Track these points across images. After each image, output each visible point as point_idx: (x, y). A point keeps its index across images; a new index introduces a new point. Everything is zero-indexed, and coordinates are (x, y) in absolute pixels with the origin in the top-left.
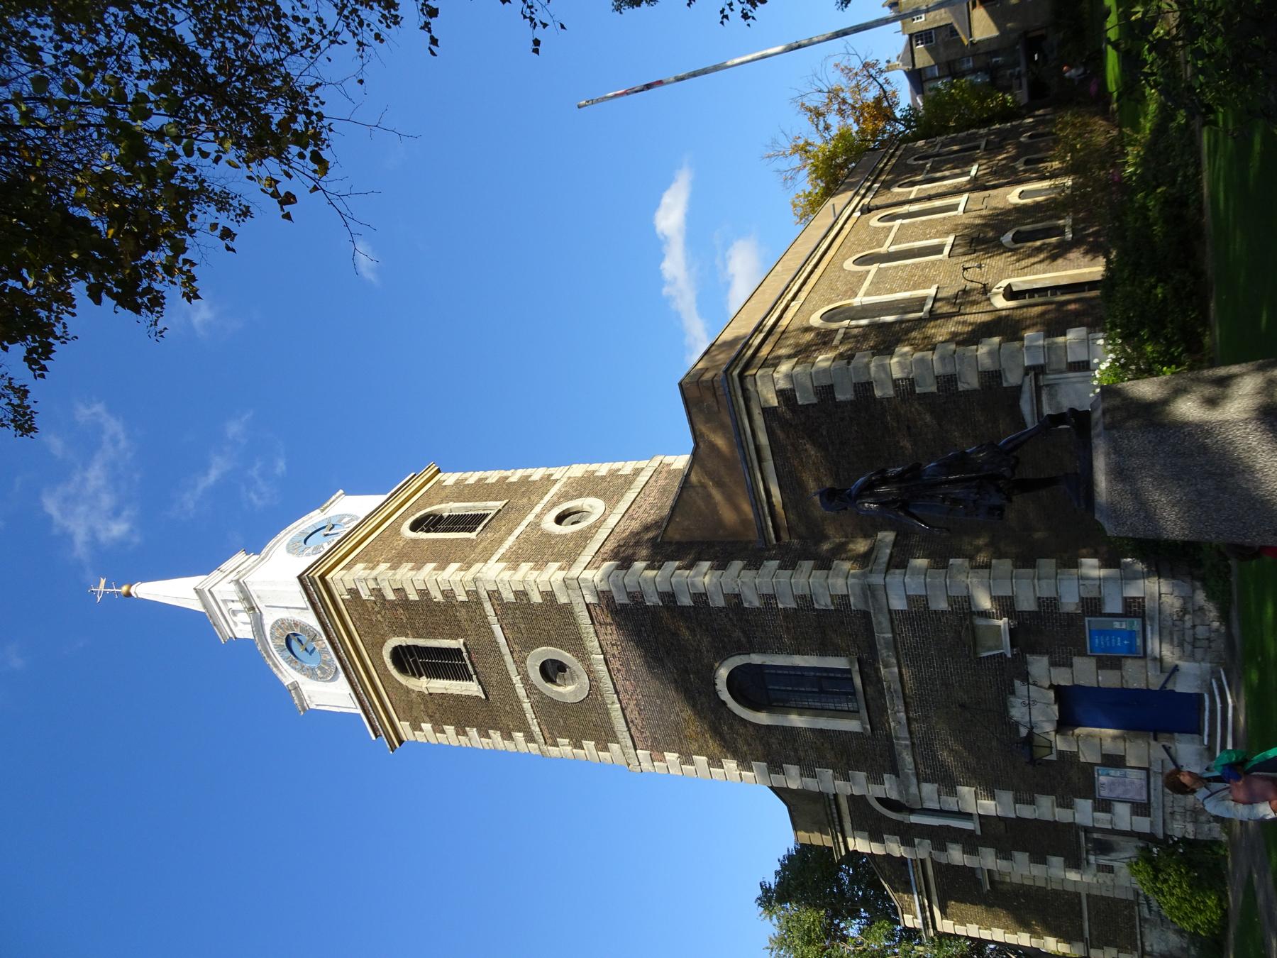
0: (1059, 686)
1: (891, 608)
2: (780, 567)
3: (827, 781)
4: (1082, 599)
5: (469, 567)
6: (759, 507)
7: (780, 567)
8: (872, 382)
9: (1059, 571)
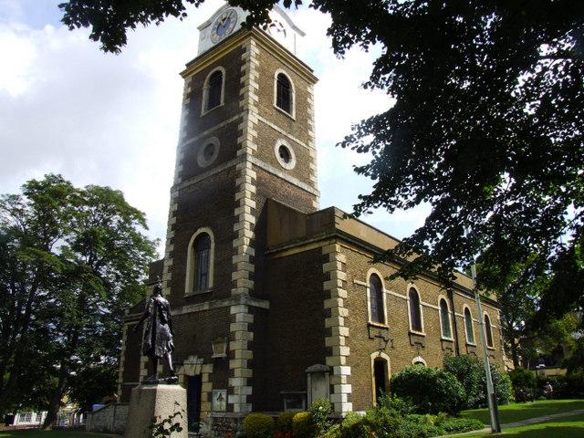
3: (167, 276)
5: (256, 106)
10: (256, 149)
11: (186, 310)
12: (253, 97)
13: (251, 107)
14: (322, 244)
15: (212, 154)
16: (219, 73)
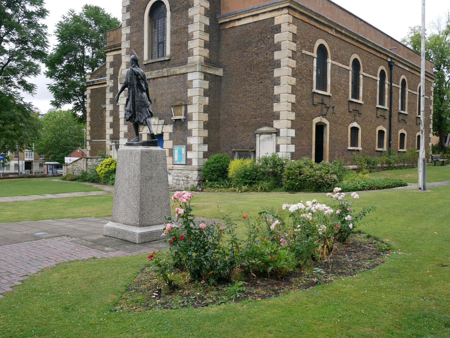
0: (163, 135)
1: (188, 74)
2: (205, 25)
4: (192, 145)
6: (233, 16)
7: (205, 25)
8: (280, 67)
9: (202, 138)
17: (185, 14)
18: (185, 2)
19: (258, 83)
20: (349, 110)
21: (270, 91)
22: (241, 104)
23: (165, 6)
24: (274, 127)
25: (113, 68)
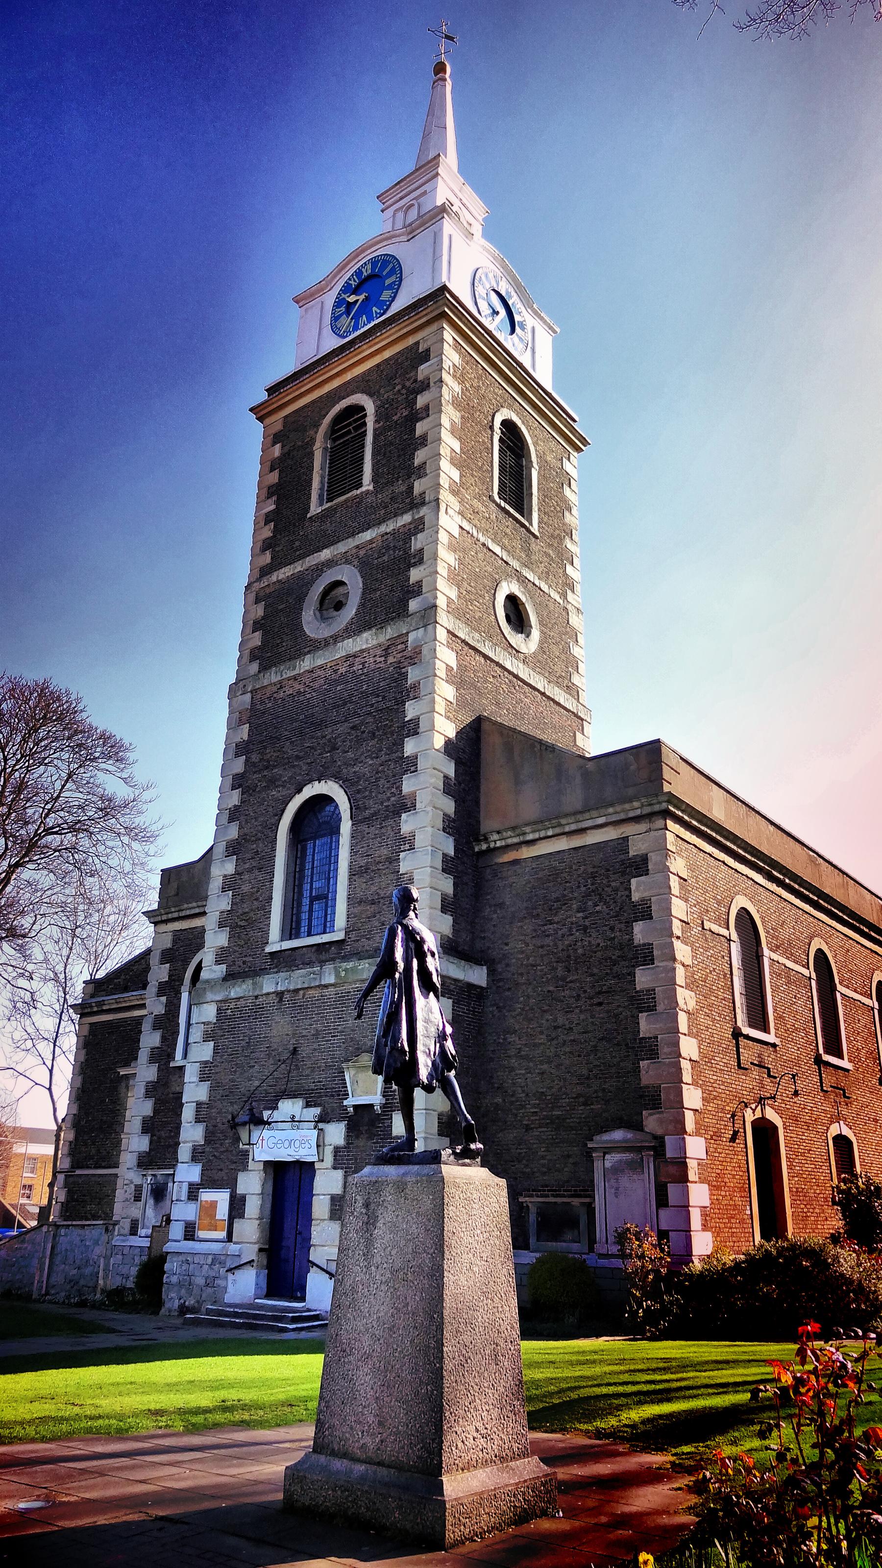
10: (453, 597)
11: (269, 984)
12: (449, 473)
13: (445, 496)
14: (629, 830)
15: (339, 606)
16: (359, 409)
17: (392, 827)
18: (393, 799)
19: (592, 1005)
20: (822, 1086)
21: (625, 1029)
22: (541, 1063)
23: (337, 806)
24: (646, 1129)
25: (168, 965)
